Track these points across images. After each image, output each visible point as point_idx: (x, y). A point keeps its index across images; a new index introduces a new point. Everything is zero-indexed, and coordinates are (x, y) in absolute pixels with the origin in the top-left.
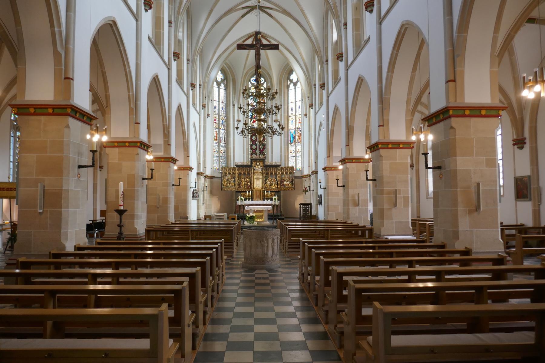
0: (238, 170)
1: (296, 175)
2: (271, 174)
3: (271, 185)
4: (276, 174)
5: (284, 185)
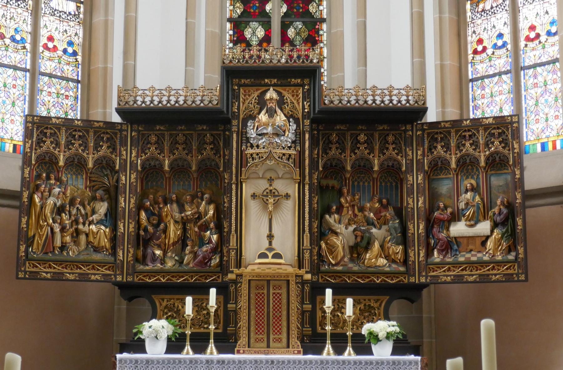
0: (141, 144)
1: (536, 177)
2: (363, 168)
3: (359, 248)
4: (393, 175)
5: (451, 245)
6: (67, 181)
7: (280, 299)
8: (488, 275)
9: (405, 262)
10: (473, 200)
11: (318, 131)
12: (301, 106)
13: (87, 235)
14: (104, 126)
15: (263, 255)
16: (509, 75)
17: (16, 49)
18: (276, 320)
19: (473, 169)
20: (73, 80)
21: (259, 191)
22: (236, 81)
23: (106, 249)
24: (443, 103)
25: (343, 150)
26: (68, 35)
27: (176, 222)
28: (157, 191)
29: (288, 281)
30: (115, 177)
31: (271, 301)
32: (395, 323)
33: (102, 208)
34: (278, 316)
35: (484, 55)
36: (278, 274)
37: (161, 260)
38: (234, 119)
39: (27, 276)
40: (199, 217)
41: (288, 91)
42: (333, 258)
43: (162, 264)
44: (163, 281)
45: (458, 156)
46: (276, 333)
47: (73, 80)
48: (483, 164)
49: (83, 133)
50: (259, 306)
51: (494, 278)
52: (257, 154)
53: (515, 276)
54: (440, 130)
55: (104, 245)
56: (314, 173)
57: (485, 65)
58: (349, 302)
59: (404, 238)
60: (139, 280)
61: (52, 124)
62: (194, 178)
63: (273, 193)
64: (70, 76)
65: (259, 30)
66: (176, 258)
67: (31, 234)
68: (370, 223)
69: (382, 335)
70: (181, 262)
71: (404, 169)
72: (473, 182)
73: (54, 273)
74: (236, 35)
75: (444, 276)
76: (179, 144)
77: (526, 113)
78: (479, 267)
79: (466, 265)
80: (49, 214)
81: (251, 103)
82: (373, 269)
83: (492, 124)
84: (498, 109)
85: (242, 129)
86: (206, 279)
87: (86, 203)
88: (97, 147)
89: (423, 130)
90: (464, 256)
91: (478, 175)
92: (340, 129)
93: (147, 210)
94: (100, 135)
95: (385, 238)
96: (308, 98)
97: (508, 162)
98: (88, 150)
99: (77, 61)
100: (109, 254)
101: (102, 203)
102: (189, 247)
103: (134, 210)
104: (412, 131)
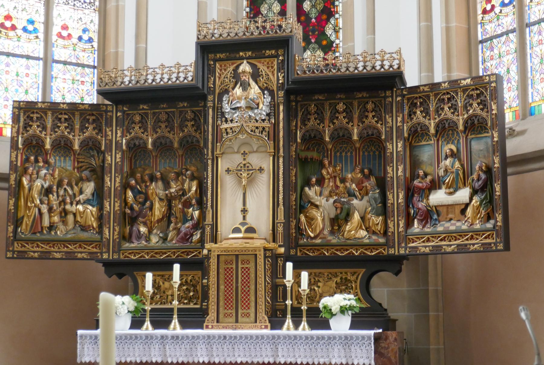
0: (126, 124)
2: (342, 138)
3: (338, 221)
4: (374, 143)
5: (429, 215)
6: (55, 163)
7: (249, 274)
8: (466, 245)
9: (385, 233)
10: (452, 167)
11: (297, 102)
12: (276, 78)
13: (75, 215)
14: (90, 108)
15: (236, 230)
16: (515, 34)
17: (29, 39)
18: (245, 295)
19: (453, 134)
20: (89, 66)
21: (233, 167)
22: (211, 56)
23: (93, 228)
24: (449, 68)
25: (322, 121)
26: (83, 23)
27: (161, 200)
28: (145, 170)
29: (256, 255)
30: (101, 157)
31: (240, 276)
32: (352, 296)
33: (89, 188)
34: (247, 291)
35: (492, 14)
36: (245, 249)
37: (146, 237)
38: (210, 95)
39: (15, 256)
40: (183, 193)
41: (263, 63)
42: (312, 232)
43: (147, 241)
44: (147, 257)
45: (437, 121)
46: (245, 308)
47: (89, 66)
48: (461, 127)
49: (69, 116)
50: (228, 281)
51: (472, 248)
52: (231, 129)
53: (493, 245)
54: (420, 95)
55: (90, 224)
56: (292, 145)
57: (494, 25)
58: (305, 275)
59: (384, 210)
60: (125, 257)
61: (38, 109)
62: (179, 155)
63: (246, 167)
64: (86, 63)
65: (275, 5)
66: (161, 235)
67: (20, 215)
68: (351, 194)
69: (335, 309)
70: (165, 239)
71: (383, 137)
72: (454, 148)
73: (41, 252)
74: (253, 12)
75: (423, 246)
76: (162, 122)
77: (531, 72)
78: (458, 237)
79: (445, 235)
80: (36, 196)
81: (227, 77)
82: (352, 241)
83: (471, 85)
84: (506, 70)
85: (218, 104)
86: (188, 255)
87: (74, 184)
88: (83, 129)
89: (403, 96)
90: (443, 225)
91: (458, 140)
92: (318, 99)
93: (133, 189)
94: (86, 117)
95: (366, 209)
96: (282, 69)
97: (487, 124)
98: (74, 132)
99: (93, 47)
100: (97, 232)
101: (88, 184)
102: (172, 224)
103: (119, 189)
104: (392, 97)
